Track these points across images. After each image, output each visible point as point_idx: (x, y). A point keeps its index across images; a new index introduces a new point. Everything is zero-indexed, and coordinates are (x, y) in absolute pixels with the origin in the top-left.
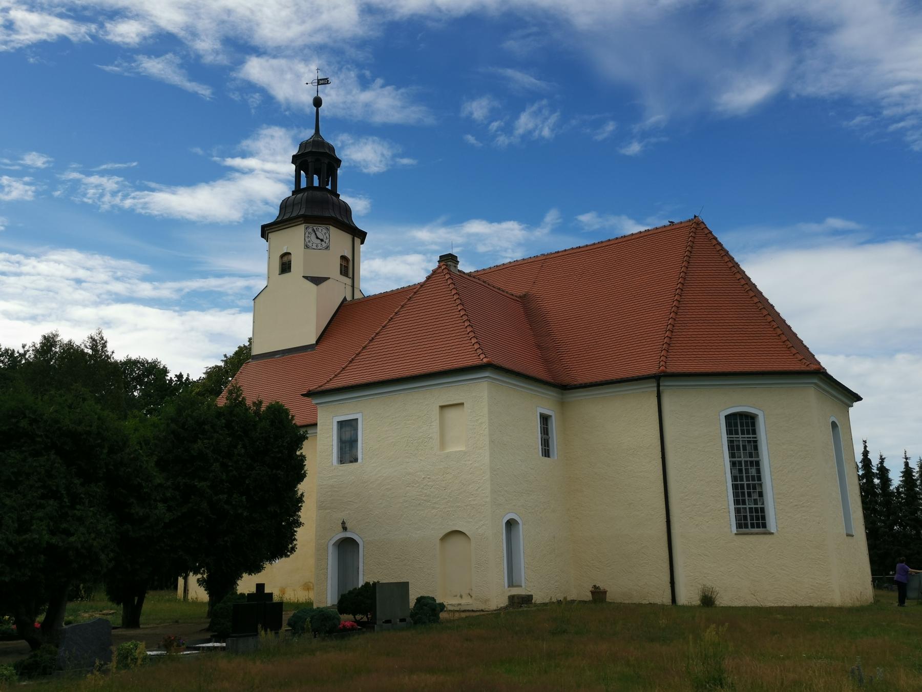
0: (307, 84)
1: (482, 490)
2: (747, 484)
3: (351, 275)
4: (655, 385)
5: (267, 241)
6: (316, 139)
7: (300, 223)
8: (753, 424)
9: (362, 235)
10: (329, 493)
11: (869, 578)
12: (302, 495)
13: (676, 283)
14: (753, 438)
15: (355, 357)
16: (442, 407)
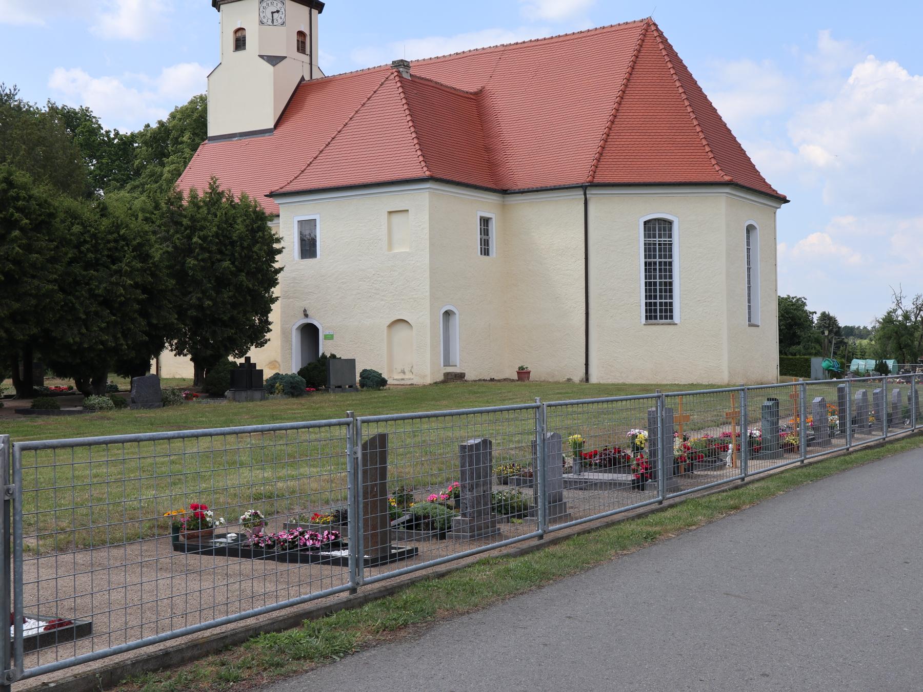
4: (582, 193)
5: (219, 11)
8: (670, 230)
10: (292, 285)
11: (777, 361)
12: (255, 201)
14: (669, 241)
16: (390, 213)
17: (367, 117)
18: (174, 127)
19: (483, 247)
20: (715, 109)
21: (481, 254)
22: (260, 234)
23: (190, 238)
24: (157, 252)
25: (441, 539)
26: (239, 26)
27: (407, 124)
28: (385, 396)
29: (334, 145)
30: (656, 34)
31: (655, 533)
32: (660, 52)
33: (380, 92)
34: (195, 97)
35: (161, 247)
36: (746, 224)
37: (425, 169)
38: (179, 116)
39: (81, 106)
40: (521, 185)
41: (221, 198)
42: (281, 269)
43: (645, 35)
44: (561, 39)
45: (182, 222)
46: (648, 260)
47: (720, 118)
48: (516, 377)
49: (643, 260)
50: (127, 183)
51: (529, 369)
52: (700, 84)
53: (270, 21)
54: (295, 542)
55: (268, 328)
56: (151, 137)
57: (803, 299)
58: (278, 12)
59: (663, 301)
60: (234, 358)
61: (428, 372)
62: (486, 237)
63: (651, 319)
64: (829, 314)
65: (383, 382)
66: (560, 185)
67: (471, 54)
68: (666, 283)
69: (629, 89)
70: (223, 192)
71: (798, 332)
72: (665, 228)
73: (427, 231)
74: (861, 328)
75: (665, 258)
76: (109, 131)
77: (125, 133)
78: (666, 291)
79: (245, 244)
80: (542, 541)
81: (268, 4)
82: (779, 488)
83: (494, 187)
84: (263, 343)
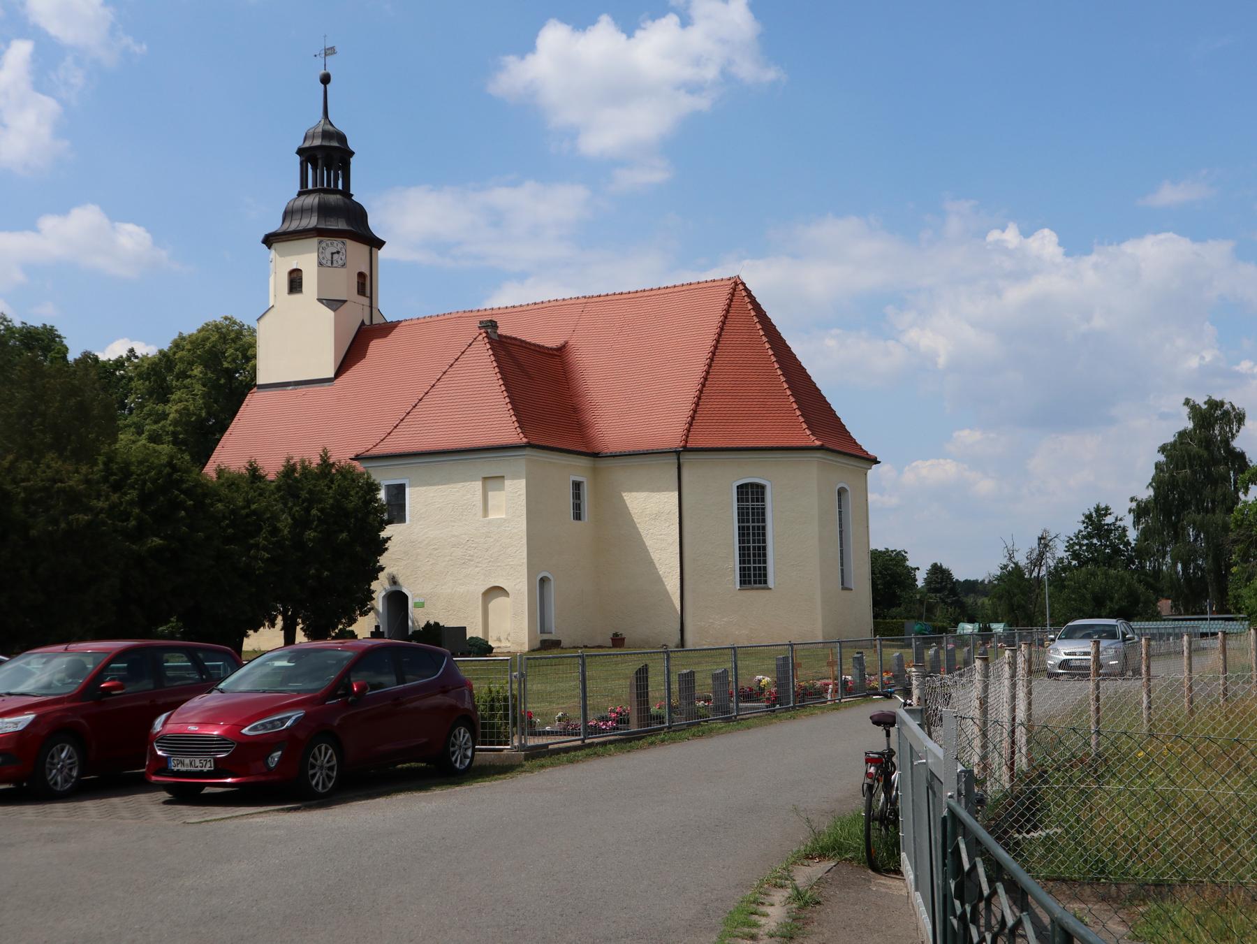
2: (750, 543)
3: (368, 293)
8: (763, 493)
9: (379, 244)
15: (399, 423)
16: (485, 479)
23: (308, 510)
26: (295, 267)
33: (468, 353)
34: (206, 324)
37: (521, 435)
40: (614, 448)
42: (389, 539)
43: (733, 295)
52: (788, 343)
53: (329, 262)
56: (148, 368)
57: (903, 553)
58: (338, 252)
62: (578, 502)
63: (745, 583)
64: (941, 566)
65: (490, 649)
68: (759, 547)
70: (334, 463)
71: (898, 592)
72: (757, 492)
73: (524, 497)
74: (986, 582)
78: (759, 556)
81: (327, 245)
83: (584, 450)
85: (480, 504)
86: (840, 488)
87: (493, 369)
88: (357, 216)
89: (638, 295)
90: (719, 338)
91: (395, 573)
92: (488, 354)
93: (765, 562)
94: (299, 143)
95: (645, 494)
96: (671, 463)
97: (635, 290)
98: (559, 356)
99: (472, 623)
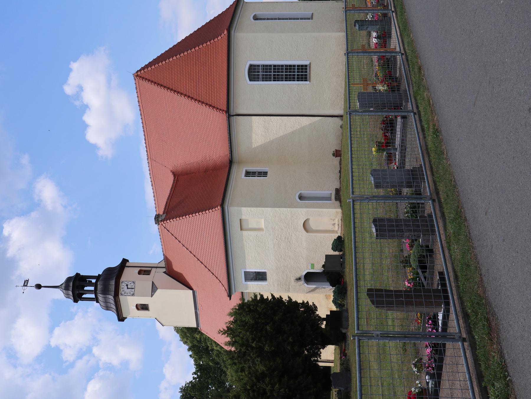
0: (23, 293)
1: (284, 212)
3: (150, 269)
4: (232, 117)
5: (127, 318)
6: (63, 288)
7: (118, 299)
8: (255, 66)
9: (125, 261)
10: (281, 286)
12: (233, 309)
13: (174, 94)
14: (261, 67)
16: (241, 229)
17: (186, 240)
18: (191, 342)
19: (262, 175)
20: (186, 38)
21: (266, 176)
22: (251, 307)
23: (252, 348)
24: (261, 368)
25: (433, 252)
26: (135, 307)
27: (191, 218)
28: (348, 239)
29: (202, 259)
30: (142, 72)
31: (434, 128)
32: (153, 70)
33: (172, 232)
34: (175, 330)
35: (257, 365)
36: (253, 20)
37: (216, 209)
38: (185, 340)
39: (179, 392)
40: (227, 152)
41: (231, 328)
42: (272, 295)
43: (143, 78)
44: (145, 126)
45: (244, 352)
46: (272, 79)
47: (191, 34)
48: (339, 158)
49: (272, 82)
50: (223, 370)
51: (334, 150)
54: (432, 346)
55: (306, 303)
56: (197, 355)
58: (127, 285)
59: (296, 70)
60: (323, 324)
61: (334, 210)
62: (257, 173)
63: (306, 78)
65: (339, 238)
66: (228, 130)
67: (152, 177)
69: (173, 88)
70: (227, 327)
73: (252, 209)
75: (271, 69)
76: (193, 377)
77: (195, 368)
78: (291, 69)
79: (257, 316)
80: (437, 200)
81: (123, 291)
82: (409, 36)
84: (315, 306)
85: (256, 233)
86: (253, 19)
87: (181, 220)
88: (109, 272)
89: (145, 130)
90: (163, 86)
91: (294, 278)
92: (173, 222)
93: (294, 66)
94: (71, 301)
95: (253, 135)
96: (234, 119)
97: (143, 132)
98: (178, 176)
99: (324, 238)
